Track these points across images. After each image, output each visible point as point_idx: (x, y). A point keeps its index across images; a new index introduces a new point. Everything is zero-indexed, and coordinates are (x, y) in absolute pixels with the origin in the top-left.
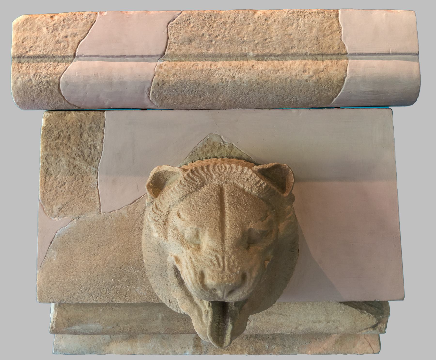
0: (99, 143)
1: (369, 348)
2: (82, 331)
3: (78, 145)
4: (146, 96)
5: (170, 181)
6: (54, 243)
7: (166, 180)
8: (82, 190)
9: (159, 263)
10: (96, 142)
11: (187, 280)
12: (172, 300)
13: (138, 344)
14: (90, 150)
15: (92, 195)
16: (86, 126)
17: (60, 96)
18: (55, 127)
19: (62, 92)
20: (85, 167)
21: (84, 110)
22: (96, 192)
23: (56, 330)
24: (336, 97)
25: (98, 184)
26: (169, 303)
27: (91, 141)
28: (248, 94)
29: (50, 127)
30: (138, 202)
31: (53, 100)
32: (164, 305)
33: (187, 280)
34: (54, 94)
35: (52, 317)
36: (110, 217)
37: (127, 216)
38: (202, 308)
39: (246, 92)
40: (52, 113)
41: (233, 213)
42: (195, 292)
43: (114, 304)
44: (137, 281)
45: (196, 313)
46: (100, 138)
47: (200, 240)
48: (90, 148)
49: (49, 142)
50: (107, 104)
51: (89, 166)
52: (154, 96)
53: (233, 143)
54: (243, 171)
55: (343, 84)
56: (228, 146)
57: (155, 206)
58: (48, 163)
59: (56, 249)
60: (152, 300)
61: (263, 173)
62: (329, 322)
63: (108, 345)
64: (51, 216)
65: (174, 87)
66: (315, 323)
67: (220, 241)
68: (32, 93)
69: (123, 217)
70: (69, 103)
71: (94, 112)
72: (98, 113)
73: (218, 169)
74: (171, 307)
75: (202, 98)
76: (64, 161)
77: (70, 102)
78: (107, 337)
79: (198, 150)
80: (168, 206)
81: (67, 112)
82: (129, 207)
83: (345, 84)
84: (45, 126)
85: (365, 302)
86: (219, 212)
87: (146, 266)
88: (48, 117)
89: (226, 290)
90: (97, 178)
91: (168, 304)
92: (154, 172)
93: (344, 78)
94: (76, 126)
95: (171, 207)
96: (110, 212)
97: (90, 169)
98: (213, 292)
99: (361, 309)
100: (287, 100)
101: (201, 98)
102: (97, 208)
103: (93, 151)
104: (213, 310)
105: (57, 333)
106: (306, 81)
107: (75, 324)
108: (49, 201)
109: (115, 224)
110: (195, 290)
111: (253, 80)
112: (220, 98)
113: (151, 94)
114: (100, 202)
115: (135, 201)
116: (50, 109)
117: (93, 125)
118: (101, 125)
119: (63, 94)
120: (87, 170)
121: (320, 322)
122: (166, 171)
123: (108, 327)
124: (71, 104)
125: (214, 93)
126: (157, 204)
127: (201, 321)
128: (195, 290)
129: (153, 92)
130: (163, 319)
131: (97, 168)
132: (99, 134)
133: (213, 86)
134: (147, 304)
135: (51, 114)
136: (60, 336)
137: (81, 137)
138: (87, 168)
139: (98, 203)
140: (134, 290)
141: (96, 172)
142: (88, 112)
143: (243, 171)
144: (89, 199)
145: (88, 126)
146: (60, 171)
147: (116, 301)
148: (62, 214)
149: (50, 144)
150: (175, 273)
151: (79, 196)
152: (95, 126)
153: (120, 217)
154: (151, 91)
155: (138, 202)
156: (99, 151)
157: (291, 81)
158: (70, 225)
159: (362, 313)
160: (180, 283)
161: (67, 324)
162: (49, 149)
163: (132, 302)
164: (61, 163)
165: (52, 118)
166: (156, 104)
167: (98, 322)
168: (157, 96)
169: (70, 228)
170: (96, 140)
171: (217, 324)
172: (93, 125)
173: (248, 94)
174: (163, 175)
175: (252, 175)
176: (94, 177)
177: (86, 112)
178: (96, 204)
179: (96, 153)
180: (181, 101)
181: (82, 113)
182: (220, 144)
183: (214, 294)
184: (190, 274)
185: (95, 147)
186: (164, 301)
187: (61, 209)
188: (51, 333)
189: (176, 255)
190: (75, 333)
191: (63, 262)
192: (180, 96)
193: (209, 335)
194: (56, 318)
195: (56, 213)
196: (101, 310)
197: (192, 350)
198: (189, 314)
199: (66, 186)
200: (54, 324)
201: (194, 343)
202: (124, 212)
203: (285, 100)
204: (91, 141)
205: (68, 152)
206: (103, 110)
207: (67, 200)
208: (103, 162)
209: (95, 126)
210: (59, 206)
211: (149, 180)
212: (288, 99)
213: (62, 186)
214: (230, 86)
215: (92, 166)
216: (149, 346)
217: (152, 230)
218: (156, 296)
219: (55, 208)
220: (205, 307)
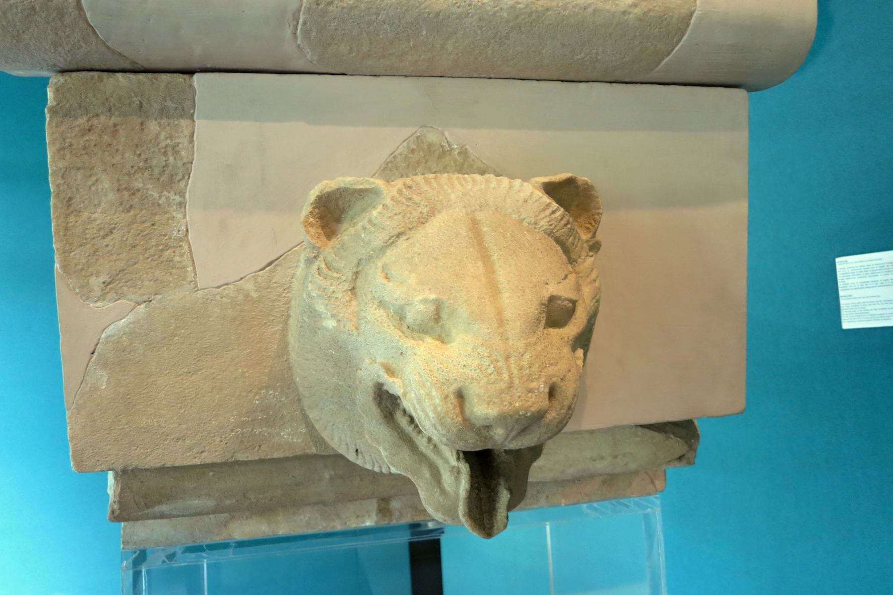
0: (185, 141)
1: (651, 486)
2: (176, 512)
3: (137, 146)
4: (288, 32)
5: (351, 213)
6: (99, 354)
7: (343, 211)
8: (153, 242)
9: (335, 380)
10: (178, 141)
11: (423, 410)
12: (362, 449)
13: (279, 518)
14: (164, 159)
15: (177, 253)
16: (151, 106)
17: (82, 25)
18: (80, 107)
19: (88, 15)
20: (156, 195)
21: (146, 71)
22: (186, 247)
23: (116, 517)
24: (669, 54)
25: (187, 230)
26: (355, 454)
27: (166, 138)
28: (507, 37)
29: (68, 106)
30: (277, 265)
31: (68, 36)
32: (341, 457)
33: (423, 410)
34: (67, 21)
35: (110, 492)
36: (218, 297)
37: (254, 295)
38: (439, 462)
39: (504, 34)
40: (70, 77)
41: (510, 266)
42: (444, 435)
43: (237, 463)
44: (282, 417)
45: (427, 474)
46: (186, 132)
47: (442, 327)
48: (165, 154)
49: (68, 141)
50: (195, 65)
51: (165, 193)
52: (307, 32)
53: (467, 147)
54: (511, 187)
55: (688, 26)
56: (457, 151)
57: (323, 266)
58: (69, 187)
59: (105, 366)
60: (314, 450)
61: (551, 189)
62: (615, 457)
63: (225, 526)
64: (88, 298)
65: (352, 13)
66: (594, 460)
67: (496, 325)
68: (9, 15)
69: (247, 296)
70: (108, 48)
71: (169, 75)
72: (180, 78)
73: (460, 183)
74: (359, 462)
75: (411, 44)
76: (106, 183)
77: (109, 44)
78: (223, 516)
79: (399, 158)
80: (356, 261)
81: (105, 74)
82: (258, 276)
83: (690, 27)
84: (55, 103)
85: (670, 423)
86: (480, 264)
87: (301, 389)
88: (59, 84)
89: (516, 426)
90: (185, 216)
91: (351, 457)
92: (317, 193)
93: (691, 14)
94: (130, 104)
95: (363, 262)
96: (219, 287)
97: (168, 198)
98: (485, 433)
99: (666, 432)
100: (579, 57)
101: (409, 42)
102: (189, 279)
103: (171, 159)
104: (471, 467)
105: (125, 520)
106: (624, 13)
107: (160, 503)
108: (79, 267)
109: (229, 311)
110: (444, 432)
111: (521, 6)
112: (450, 46)
113: (299, 27)
114: (194, 268)
115: (270, 264)
116: (62, 65)
117: (169, 103)
118: (188, 103)
119: (89, 20)
120: (160, 202)
121: (602, 458)
122: (345, 190)
123: (228, 502)
124: (113, 52)
125: (438, 32)
126: (329, 259)
127: (440, 488)
128: (444, 432)
129: (305, 23)
130: (332, 479)
131: (184, 197)
132: (184, 123)
133: (438, 14)
134: (304, 459)
135: (67, 78)
136: (131, 523)
137: (142, 130)
138: (160, 197)
139: (190, 269)
140: (279, 434)
141: (182, 205)
142: (156, 75)
143: (511, 187)
144: (170, 260)
145: (157, 106)
146: (99, 204)
147: (241, 457)
148: (112, 295)
149: (71, 145)
150: (375, 399)
151: (147, 255)
152: (174, 106)
153: (241, 297)
154: (301, 21)
155: (277, 265)
156: (185, 160)
157: (595, 11)
158: (131, 317)
159: (668, 438)
160: (385, 417)
161: (143, 504)
162: (68, 157)
163: (275, 456)
164: (100, 187)
165: (70, 85)
166: (309, 56)
167: (206, 495)
168: (314, 34)
169: (134, 323)
170: (179, 137)
171: (476, 491)
172: (169, 103)
173: (507, 37)
174: (337, 200)
175: (532, 194)
176: (180, 216)
177: (150, 75)
178: (187, 271)
179: (180, 164)
180: (365, 49)
181: (141, 77)
182: (442, 147)
183: (485, 438)
184: (431, 398)
185: (176, 153)
186: (342, 451)
187: (109, 283)
188: (112, 521)
189: (385, 361)
190: (162, 516)
191: (122, 390)
192: (365, 35)
193: (464, 516)
194: (120, 495)
195: (97, 292)
196: (211, 474)
197: (375, 518)
198: (410, 477)
199: (116, 235)
200: (116, 507)
201: (379, 506)
202: (249, 286)
203: (576, 58)
204: (166, 138)
205: (114, 161)
206: (191, 72)
207: (120, 265)
208: (195, 185)
209: (174, 106)
210: (104, 278)
211: (306, 209)
212: (582, 55)
213: (107, 235)
214: (472, 17)
215: (172, 193)
216: (301, 520)
217: (320, 315)
218: (319, 441)
219: (96, 282)
220: (446, 461)
